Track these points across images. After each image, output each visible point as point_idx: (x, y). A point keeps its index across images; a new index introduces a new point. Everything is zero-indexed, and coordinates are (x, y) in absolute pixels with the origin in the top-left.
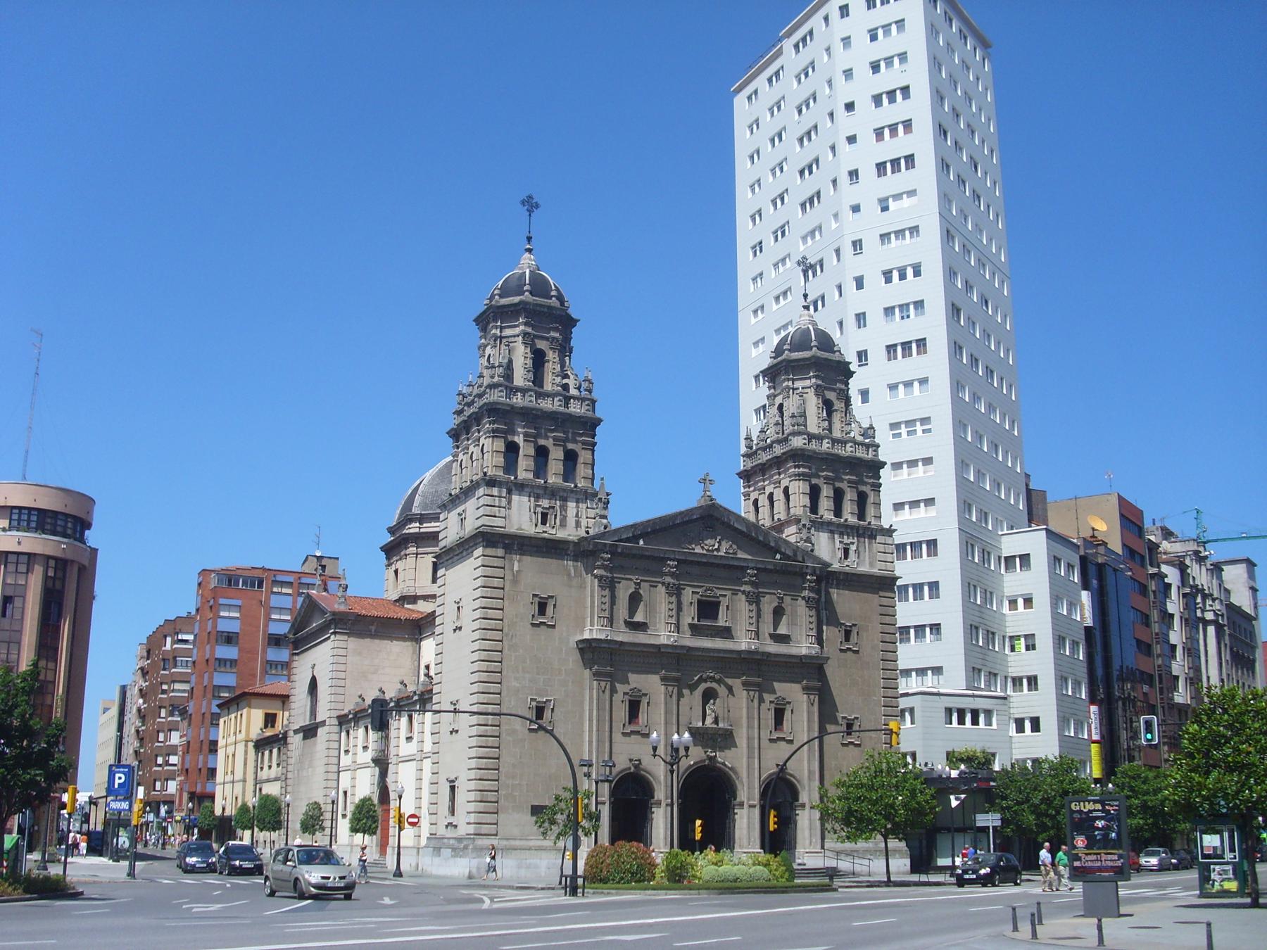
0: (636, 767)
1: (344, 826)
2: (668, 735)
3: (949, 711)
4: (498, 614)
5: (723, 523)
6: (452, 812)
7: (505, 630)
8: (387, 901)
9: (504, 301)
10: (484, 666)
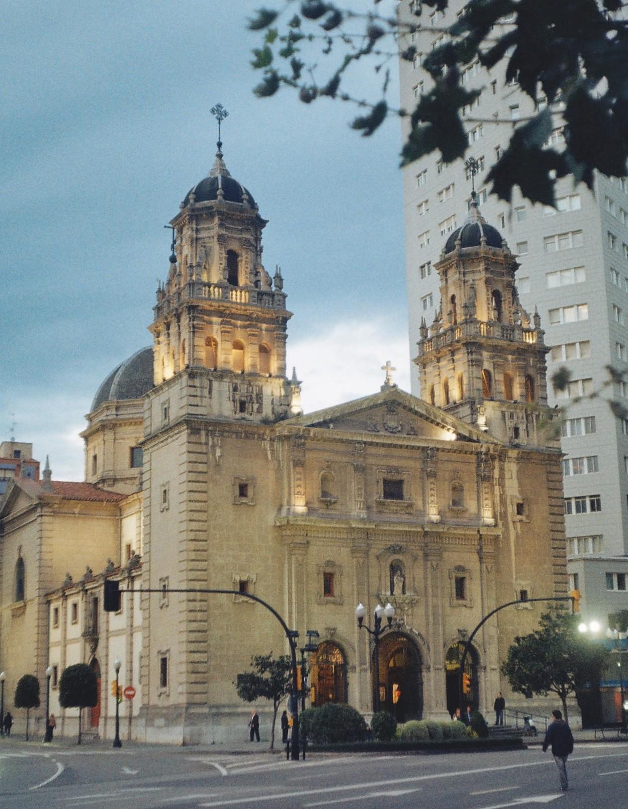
0: (332, 635)
1: (55, 696)
2: (369, 607)
3: (609, 575)
4: (202, 497)
5: (405, 407)
6: (164, 682)
7: (211, 510)
8: (127, 771)
9: (198, 205)
10: (192, 545)
